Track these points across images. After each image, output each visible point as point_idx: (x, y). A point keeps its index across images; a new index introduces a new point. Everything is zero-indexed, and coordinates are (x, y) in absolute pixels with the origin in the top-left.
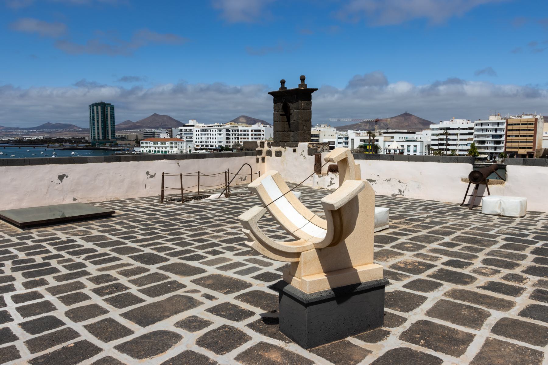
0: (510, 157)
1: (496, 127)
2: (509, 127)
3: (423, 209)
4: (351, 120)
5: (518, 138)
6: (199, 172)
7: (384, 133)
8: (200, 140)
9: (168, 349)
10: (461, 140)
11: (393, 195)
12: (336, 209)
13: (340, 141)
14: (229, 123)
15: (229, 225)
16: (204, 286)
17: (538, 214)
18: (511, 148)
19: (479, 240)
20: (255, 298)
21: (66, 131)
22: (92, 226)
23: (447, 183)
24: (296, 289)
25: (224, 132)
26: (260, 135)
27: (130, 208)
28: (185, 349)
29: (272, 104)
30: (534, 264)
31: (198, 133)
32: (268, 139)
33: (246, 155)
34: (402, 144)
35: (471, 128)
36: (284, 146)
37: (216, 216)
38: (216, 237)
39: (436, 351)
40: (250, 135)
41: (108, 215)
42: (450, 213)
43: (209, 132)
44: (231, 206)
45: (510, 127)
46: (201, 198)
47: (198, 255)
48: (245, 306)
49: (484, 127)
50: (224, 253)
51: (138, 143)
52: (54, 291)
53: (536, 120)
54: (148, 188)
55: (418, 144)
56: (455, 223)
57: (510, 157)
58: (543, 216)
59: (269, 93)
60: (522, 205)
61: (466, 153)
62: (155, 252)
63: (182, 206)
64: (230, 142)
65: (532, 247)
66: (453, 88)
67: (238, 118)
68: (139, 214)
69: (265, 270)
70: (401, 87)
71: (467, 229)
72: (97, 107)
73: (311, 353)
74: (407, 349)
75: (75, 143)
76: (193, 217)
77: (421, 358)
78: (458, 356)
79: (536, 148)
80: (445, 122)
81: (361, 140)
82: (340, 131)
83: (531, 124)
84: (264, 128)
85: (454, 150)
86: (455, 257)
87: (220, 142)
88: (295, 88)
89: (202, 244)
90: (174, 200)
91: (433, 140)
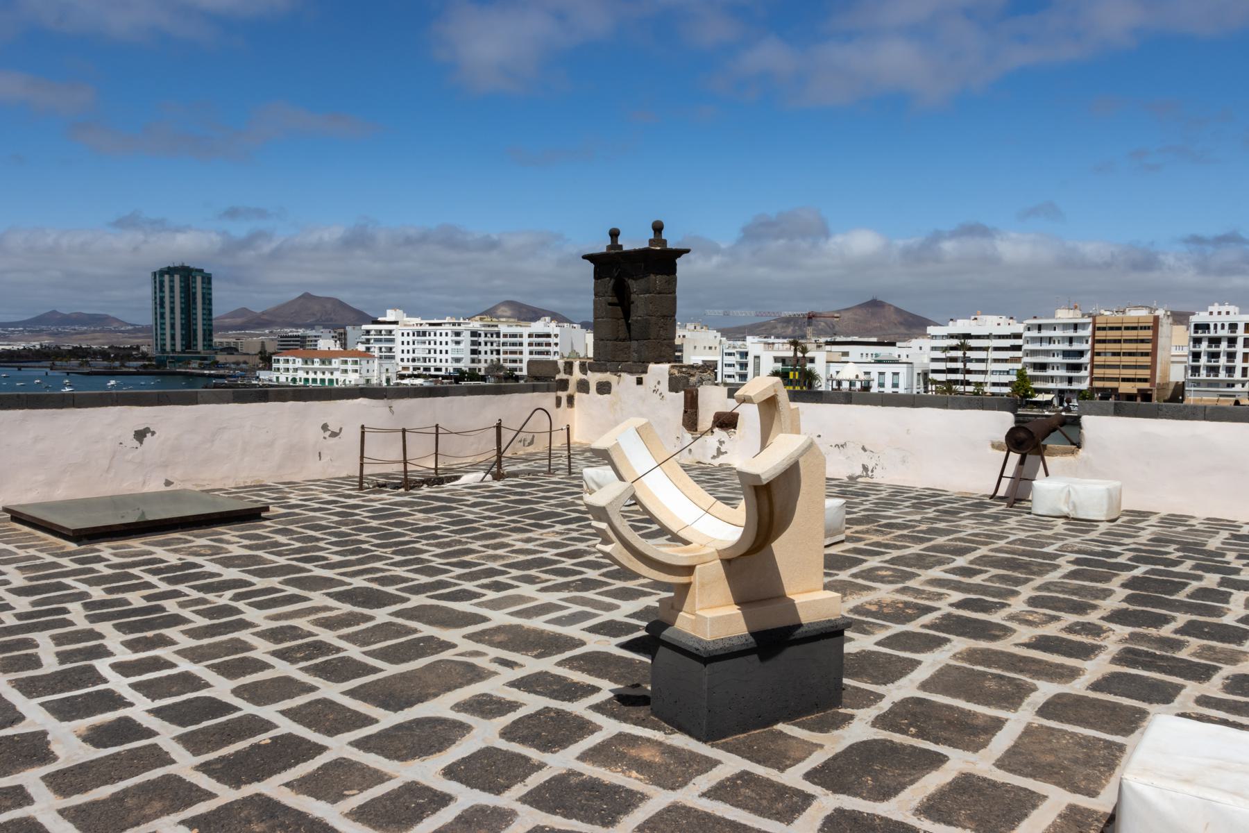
0: (1101, 398)
1: (1070, 333)
2: (1098, 333)
3: (914, 506)
4: (753, 313)
5: (1117, 358)
6: (437, 426)
7: (827, 343)
8: (411, 356)
9: (450, 745)
10: (996, 361)
11: (851, 478)
13: (729, 360)
16: (491, 644)
17: (1144, 515)
18: (1103, 379)
19: (1019, 565)
20: (596, 663)
21: (94, 332)
22: (224, 537)
23: (959, 452)
24: (685, 634)
25: (466, 338)
26: (548, 344)
27: (293, 502)
28: (483, 746)
29: (590, 283)
30: (1125, 605)
31: (406, 339)
32: (566, 355)
34: (868, 368)
35: (1018, 336)
36: (616, 371)
37: (485, 518)
38: (495, 558)
39: (937, 743)
40: (525, 344)
41: (252, 515)
42: (968, 513)
43: (432, 337)
44: (513, 498)
45: (1100, 335)
46: (440, 481)
47: (464, 591)
51: (266, 360)
52: (194, 655)
54: (325, 459)
57: (1101, 398)
58: (1153, 520)
59: (585, 257)
60: (1110, 497)
61: (1007, 390)
62: (375, 586)
63: (407, 498)
64: (480, 361)
65: (1126, 576)
66: (972, 246)
67: (495, 308)
68: (318, 514)
69: (605, 616)
70: (861, 242)
71: (1002, 543)
72: (172, 276)
74: (886, 741)
75: (116, 358)
76: (436, 519)
77: (910, 755)
78: (976, 750)
80: (960, 322)
81: (776, 359)
82: (729, 339)
83: (1145, 328)
84: (557, 331)
85: (981, 384)
86: (976, 592)
87: (458, 360)
88: (642, 247)
89: (467, 570)
90: (384, 485)
91: (934, 360)
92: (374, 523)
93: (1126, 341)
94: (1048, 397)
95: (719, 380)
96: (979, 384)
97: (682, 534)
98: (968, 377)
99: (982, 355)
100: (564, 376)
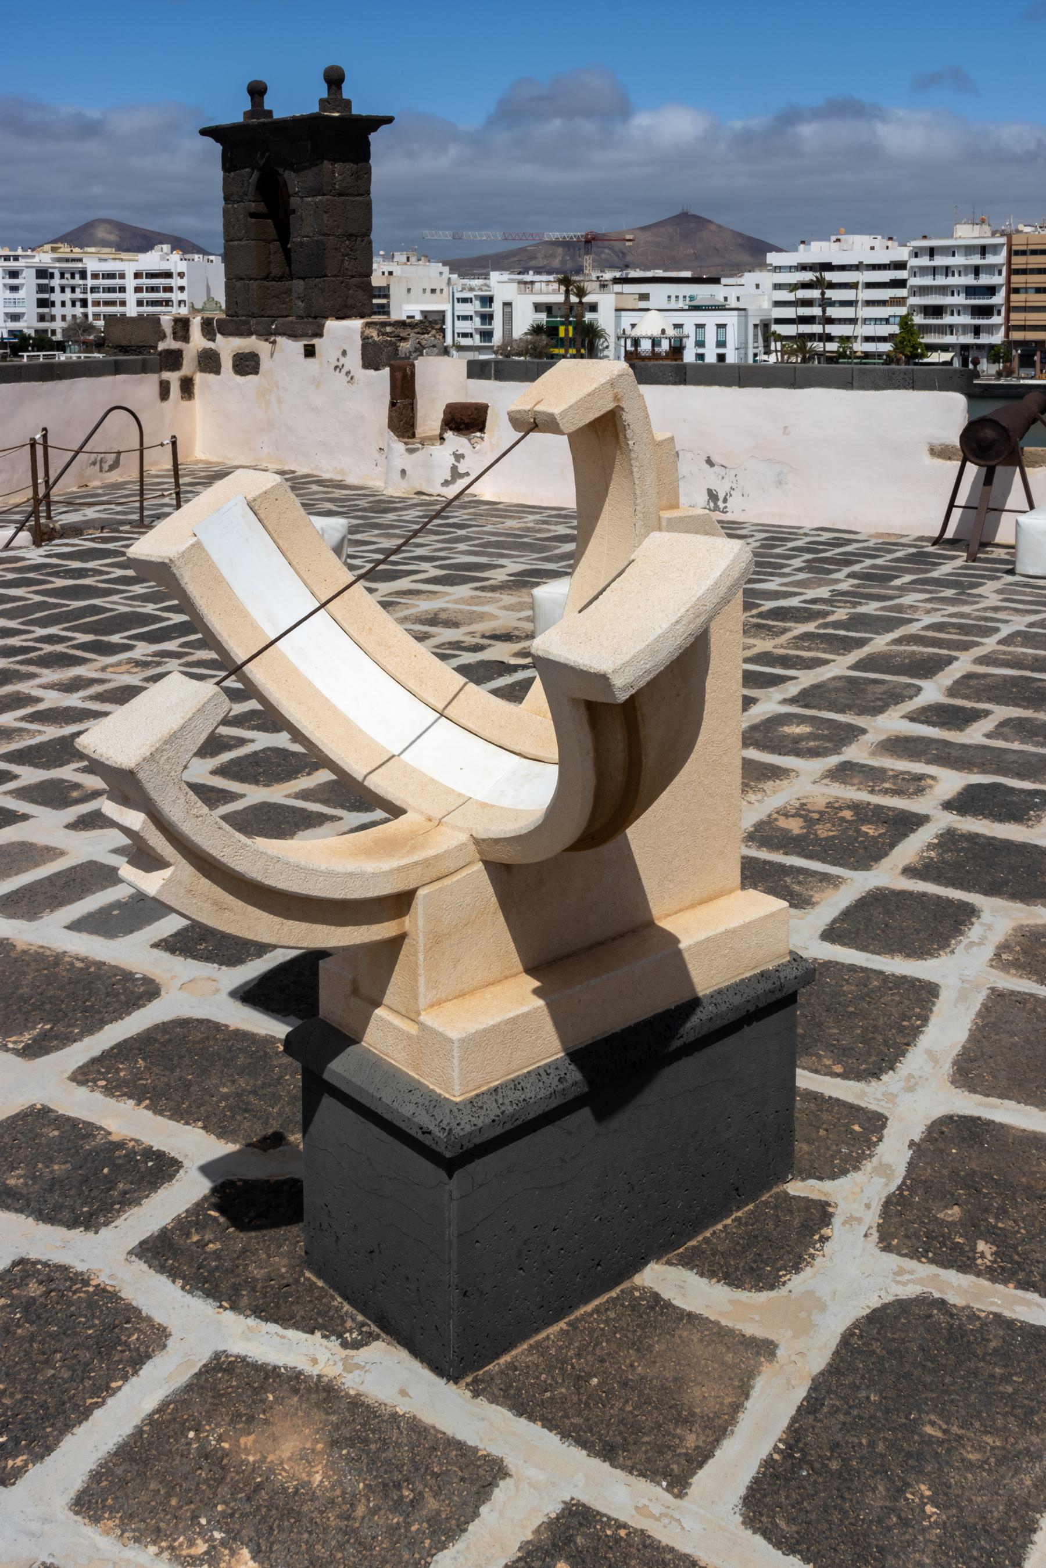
1: (976, 260)
2: (1015, 259)
3: (809, 566)
7: (616, 281)
10: (869, 303)
12: (622, 697)
14: (48, 247)
15: (50, 675)
20: (172, 1066)
24: (393, 1075)
25: (28, 281)
26: (169, 289)
29: (216, 174)
33: (117, 369)
35: (900, 266)
36: (266, 335)
42: (908, 578)
44: (60, 583)
45: (1018, 262)
48: (126, 1121)
49: (940, 261)
50: (25, 817)
55: (730, 319)
56: (936, 618)
59: (204, 132)
61: (886, 347)
64: (53, 318)
66: (843, 131)
70: (672, 125)
71: (990, 644)
73: (482, 1402)
77: (1003, 1355)
80: (815, 245)
81: (538, 307)
82: (462, 275)
85: (847, 339)
87: (15, 317)
91: (778, 304)
94: (946, 357)
95: (449, 341)
96: (845, 339)
97: (378, 783)
100: (175, 345)
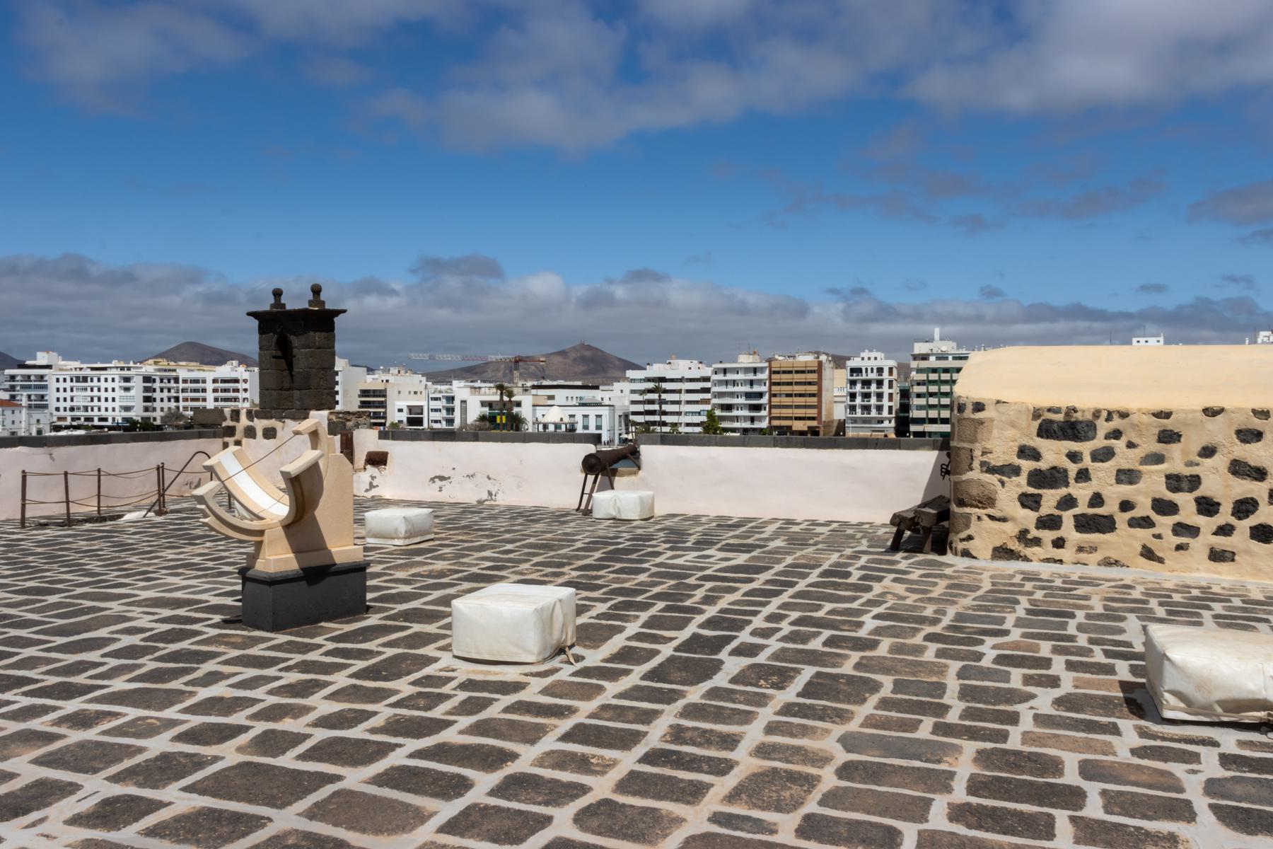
1: (751, 376)
2: (774, 376)
5: (790, 399)
6: (99, 470)
7: (534, 387)
8: (68, 404)
10: (689, 402)
11: (480, 502)
13: (434, 405)
14: (151, 361)
25: (137, 385)
26: (237, 390)
31: (61, 385)
33: (200, 436)
35: (707, 379)
43: (95, 383)
45: (776, 378)
46: (103, 519)
49: (730, 377)
53: (820, 363)
55: (604, 412)
59: (249, 314)
61: (699, 429)
64: (154, 410)
79: (824, 419)
80: (656, 366)
81: (483, 404)
84: (246, 375)
87: (127, 409)
90: (46, 525)
91: (634, 402)
92: (40, 550)
93: (797, 383)
96: (674, 425)
97: (261, 515)
98: (664, 418)
99: (675, 397)
